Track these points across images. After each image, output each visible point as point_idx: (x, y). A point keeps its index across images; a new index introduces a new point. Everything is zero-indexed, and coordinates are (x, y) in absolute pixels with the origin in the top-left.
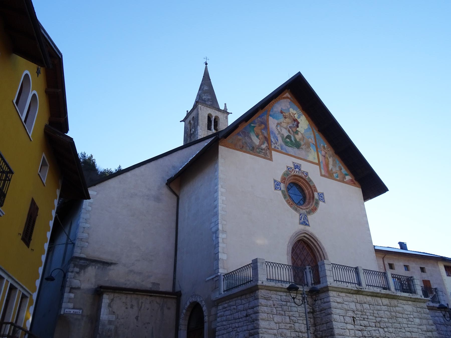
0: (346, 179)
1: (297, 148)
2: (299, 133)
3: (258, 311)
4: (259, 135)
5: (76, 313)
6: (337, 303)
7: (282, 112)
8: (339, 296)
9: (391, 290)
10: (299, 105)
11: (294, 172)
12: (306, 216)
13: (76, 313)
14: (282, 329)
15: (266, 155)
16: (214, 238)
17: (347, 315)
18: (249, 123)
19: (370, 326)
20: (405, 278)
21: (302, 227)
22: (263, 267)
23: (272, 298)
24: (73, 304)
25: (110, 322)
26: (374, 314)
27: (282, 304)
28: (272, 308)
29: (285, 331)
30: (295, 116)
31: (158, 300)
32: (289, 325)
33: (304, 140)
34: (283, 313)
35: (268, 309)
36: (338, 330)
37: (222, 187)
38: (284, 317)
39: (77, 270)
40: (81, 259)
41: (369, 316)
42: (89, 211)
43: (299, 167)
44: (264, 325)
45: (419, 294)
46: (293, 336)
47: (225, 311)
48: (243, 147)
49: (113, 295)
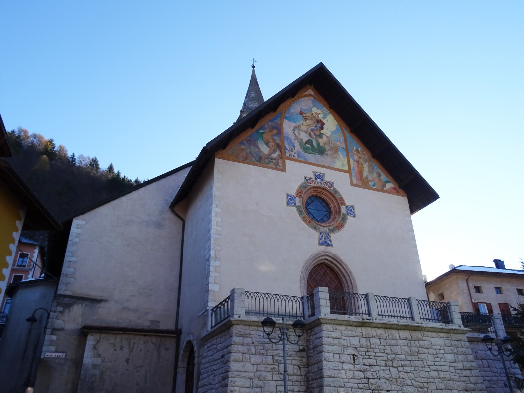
0: (386, 187)
1: (320, 155)
2: (324, 137)
3: (230, 350)
4: (269, 143)
5: (58, 357)
6: (332, 339)
7: (301, 113)
8: (336, 329)
9: (415, 321)
10: (326, 103)
11: (315, 184)
12: (328, 234)
13: (58, 357)
14: (261, 371)
15: (277, 166)
16: (207, 267)
17: (345, 352)
18: (256, 129)
19: (377, 365)
20: (441, 305)
21: (323, 248)
22: (243, 298)
23: (251, 335)
24: (55, 347)
25: (95, 366)
26: (385, 350)
27: (265, 342)
28: (250, 347)
29: (264, 374)
30: (319, 116)
31: (154, 339)
32: (271, 366)
33: (331, 144)
34: (264, 352)
35: (243, 348)
36: (329, 371)
37: (217, 207)
38: (265, 356)
39: (60, 309)
40: (65, 296)
41: (378, 352)
42: (76, 243)
43: (321, 177)
44: (236, 367)
45: (456, 323)
46: (276, 380)
47: (209, 351)
48: (247, 158)
49: (99, 335)
